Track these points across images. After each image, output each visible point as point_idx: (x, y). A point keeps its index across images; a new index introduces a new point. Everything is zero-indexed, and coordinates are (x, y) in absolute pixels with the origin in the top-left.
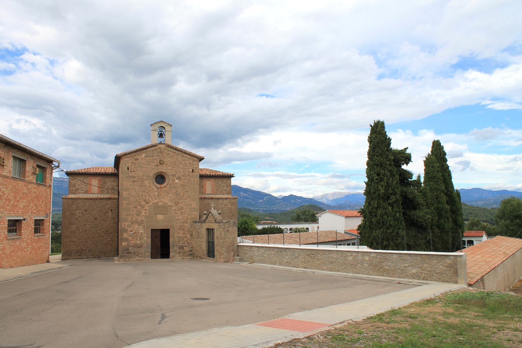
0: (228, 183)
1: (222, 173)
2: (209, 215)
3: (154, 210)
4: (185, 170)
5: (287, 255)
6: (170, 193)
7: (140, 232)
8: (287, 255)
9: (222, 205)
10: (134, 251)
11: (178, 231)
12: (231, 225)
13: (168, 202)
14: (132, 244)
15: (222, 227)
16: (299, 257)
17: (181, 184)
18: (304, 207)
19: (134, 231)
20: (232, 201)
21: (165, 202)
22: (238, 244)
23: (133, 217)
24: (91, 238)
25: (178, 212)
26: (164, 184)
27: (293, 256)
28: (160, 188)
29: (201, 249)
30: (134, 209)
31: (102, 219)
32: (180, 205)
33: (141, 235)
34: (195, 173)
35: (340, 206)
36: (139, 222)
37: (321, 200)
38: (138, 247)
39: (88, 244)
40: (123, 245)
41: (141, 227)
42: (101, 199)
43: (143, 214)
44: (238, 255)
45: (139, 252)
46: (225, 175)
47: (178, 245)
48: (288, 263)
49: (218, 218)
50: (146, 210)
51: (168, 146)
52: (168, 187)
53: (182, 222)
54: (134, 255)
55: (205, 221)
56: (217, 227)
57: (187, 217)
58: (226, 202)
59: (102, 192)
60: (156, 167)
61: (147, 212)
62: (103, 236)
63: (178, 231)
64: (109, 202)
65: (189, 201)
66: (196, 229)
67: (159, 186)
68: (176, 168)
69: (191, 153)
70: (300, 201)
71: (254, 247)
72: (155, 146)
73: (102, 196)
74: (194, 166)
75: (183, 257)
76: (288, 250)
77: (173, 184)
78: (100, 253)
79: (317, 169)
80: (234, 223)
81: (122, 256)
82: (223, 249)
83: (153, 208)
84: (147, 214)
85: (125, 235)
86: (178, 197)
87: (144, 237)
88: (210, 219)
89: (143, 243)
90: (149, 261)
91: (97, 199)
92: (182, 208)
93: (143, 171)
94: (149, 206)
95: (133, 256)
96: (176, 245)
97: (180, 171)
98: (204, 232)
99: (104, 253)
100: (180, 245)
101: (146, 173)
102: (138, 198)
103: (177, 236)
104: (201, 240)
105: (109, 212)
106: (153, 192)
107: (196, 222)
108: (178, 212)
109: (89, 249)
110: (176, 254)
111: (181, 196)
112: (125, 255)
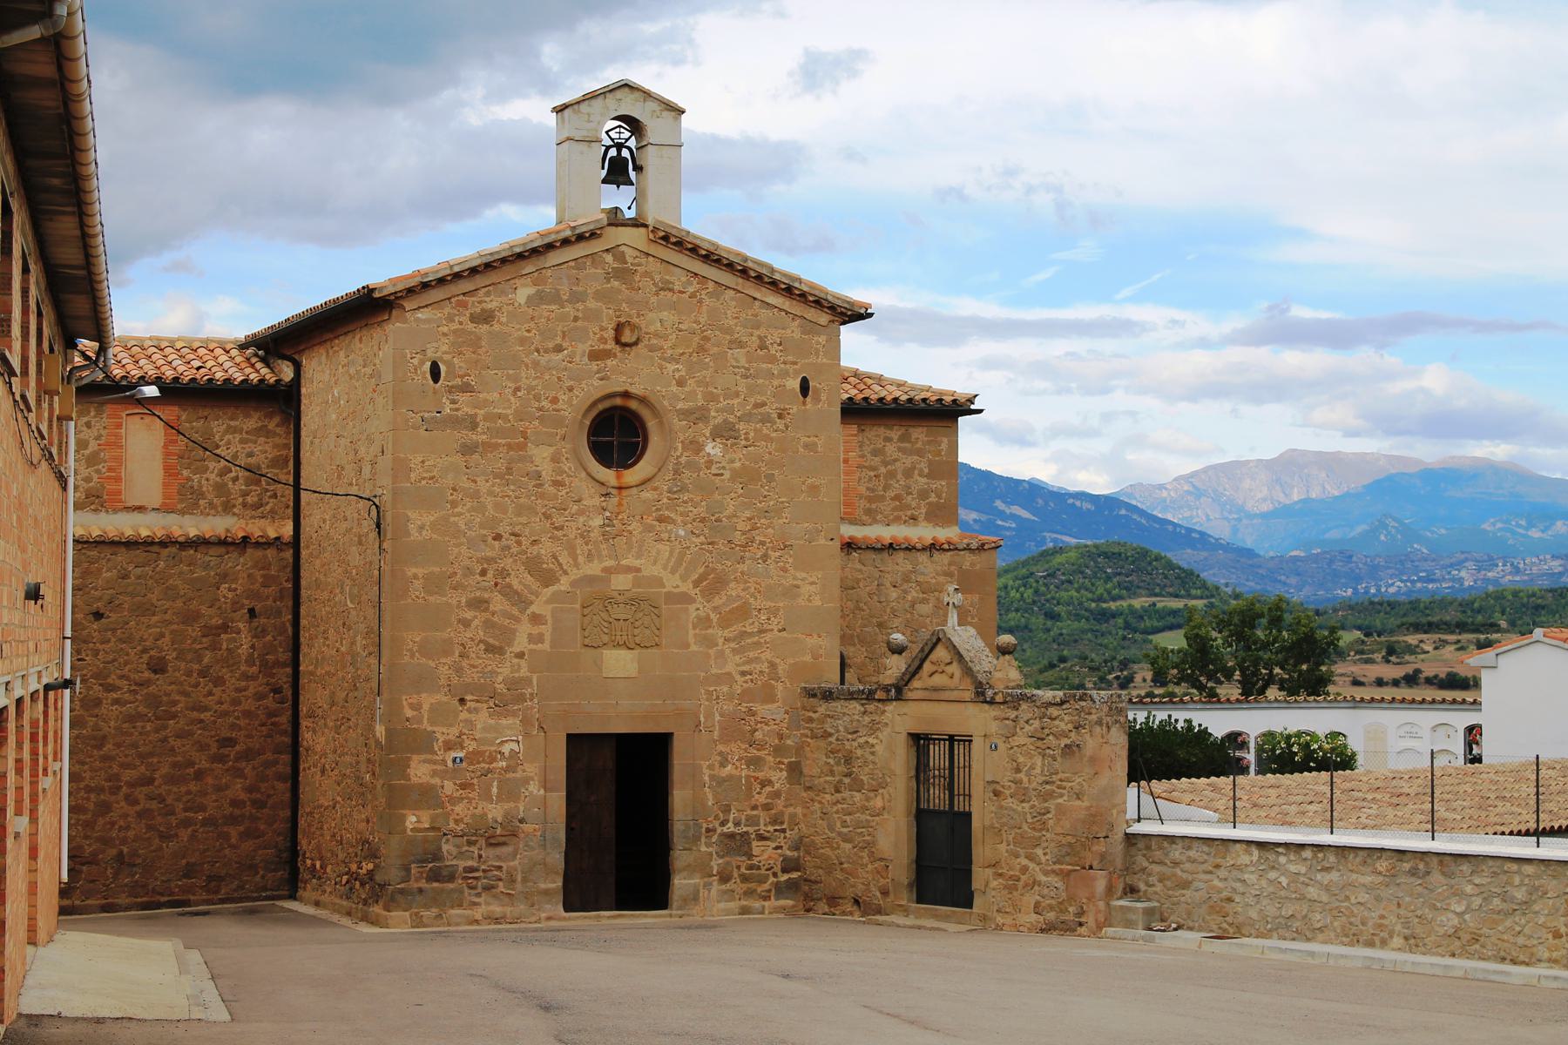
0: (939, 453)
1: (900, 385)
2: (933, 657)
3: (587, 620)
4: (761, 381)
5: (1459, 894)
6: (673, 522)
7: (506, 749)
8: (1455, 894)
9: (905, 586)
10: (470, 863)
11: (721, 748)
12: (1094, 717)
13: (665, 575)
14: (457, 822)
15: (1027, 728)
16: (1536, 908)
17: (737, 465)
18: (1059, 559)
19: (472, 746)
20: (966, 566)
21: (645, 573)
22: (1129, 831)
23: (465, 663)
24: (131, 785)
25: (719, 634)
26: (641, 463)
27: (1496, 901)
28: (620, 488)
29: (865, 854)
30: (469, 615)
31: (196, 667)
32: (734, 589)
33: (507, 770)
34: (817, 400)
35: (1331, 562)
36: (501, 688)
37: (1187, 514)
38: (493, 843)
39: (113, 824)
40: (405, 831)
41: (510, 721)
42: (200, 543)
43: (521, 643)
44: (1131, 891)
45: (500, 868)
46: (924, 400)
47: (719, 830)
48: (1466, 937)
49: (998, 675)
50: (536, 619)
51: (666, 238)
52: (664, 483)
53: (746, 695)
54: (471, 888)
55: (899, 690)
56: (994, 727)
57: (773, 665)
58: (928, 566)
59: (183, 498)
60: (594, 366)
61: (546, 630)
62: (199, 775)
63: (721, 748)
64: (241, 564)
65: (784, 570)
66: (827, 735)
67: (608, 475)
68: (708, 373)
69: (800, 281)
70: (1025, 514)
71: (1238, 845)
72: (594, 235)
73: (191, 526)
74: (812, 359)
75: (744, 903)
76: (1466, 868)
77: (691, 465)
78: (186, 876)
79: (1158, 276)
80: (1111, 709)
81: (402, 892)
82: (1031, 858)
83: (578, 606)
84: (546, 646)
85: (420, 771)
86: (722, 545)
87: (526, 781)
88: (938, 680)
89: (521, 815)
90: (553, 923)
91: (166, 543)
92: (743, 612)
93: (518, 389)
94: (555, 598)
95: (462, 892)
96: (708, 830)
97: (734, 389)
98: (895, 759)
99: (210, 878)
100: (729, 827)
101: (537, 398)
102: (493, 548)
103: (712, 777)
104: (868, 799)
105: (241, 625)
106: (581, 512)
107: (828, 696)
108: (720, 633)
109: (121, 853)
110: (707, 886)
111: (738, 538)
112: (416, 885)
